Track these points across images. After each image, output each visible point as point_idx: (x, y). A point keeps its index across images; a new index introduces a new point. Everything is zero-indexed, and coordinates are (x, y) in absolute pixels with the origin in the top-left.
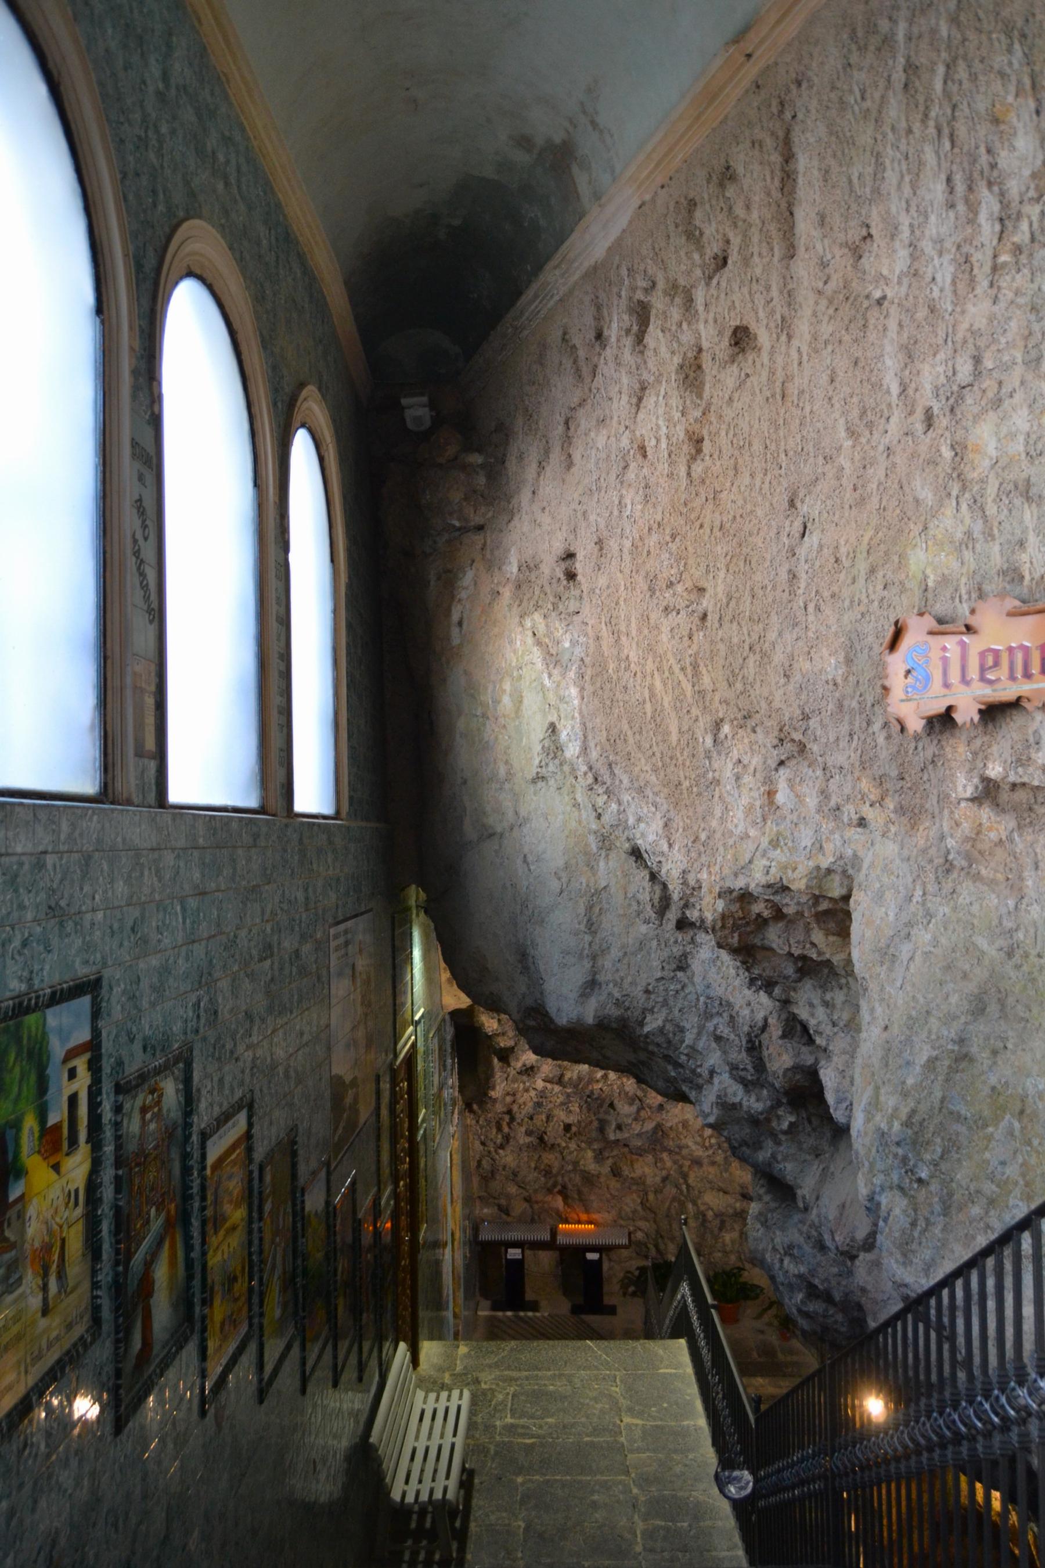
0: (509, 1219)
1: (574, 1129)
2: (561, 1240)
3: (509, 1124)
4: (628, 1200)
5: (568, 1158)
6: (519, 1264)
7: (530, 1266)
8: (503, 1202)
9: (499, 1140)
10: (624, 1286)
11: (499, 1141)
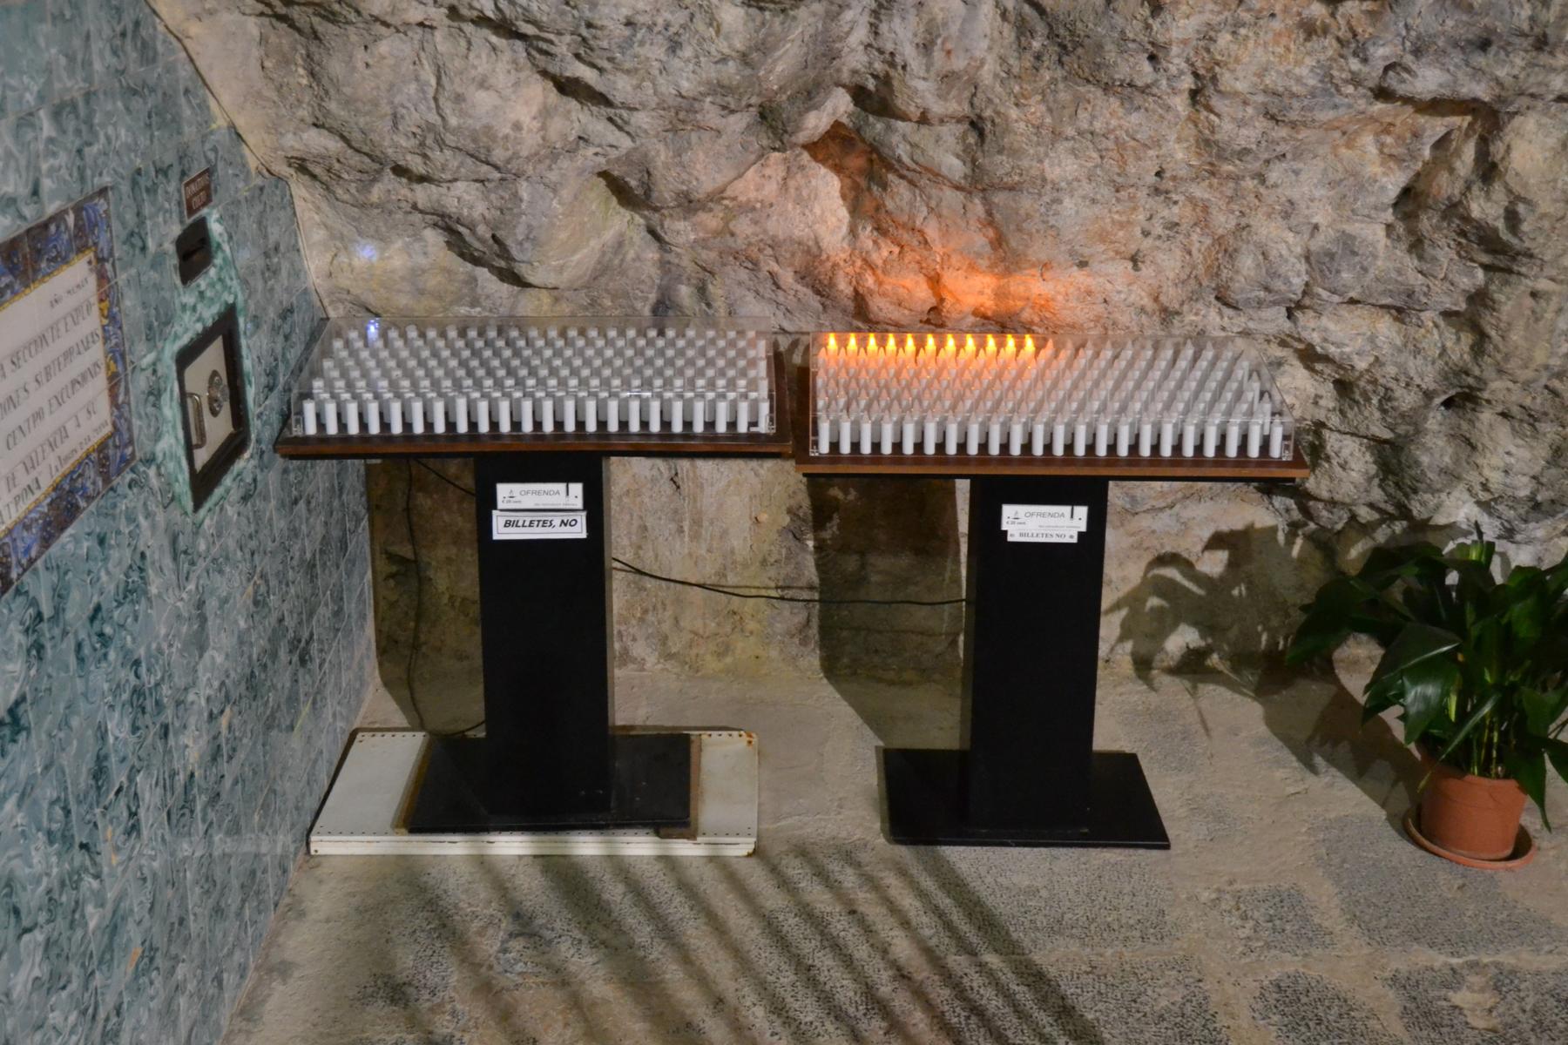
0: (528, 304)
2: (838, 428)
6: (576, 570)
10: (1146, 631)
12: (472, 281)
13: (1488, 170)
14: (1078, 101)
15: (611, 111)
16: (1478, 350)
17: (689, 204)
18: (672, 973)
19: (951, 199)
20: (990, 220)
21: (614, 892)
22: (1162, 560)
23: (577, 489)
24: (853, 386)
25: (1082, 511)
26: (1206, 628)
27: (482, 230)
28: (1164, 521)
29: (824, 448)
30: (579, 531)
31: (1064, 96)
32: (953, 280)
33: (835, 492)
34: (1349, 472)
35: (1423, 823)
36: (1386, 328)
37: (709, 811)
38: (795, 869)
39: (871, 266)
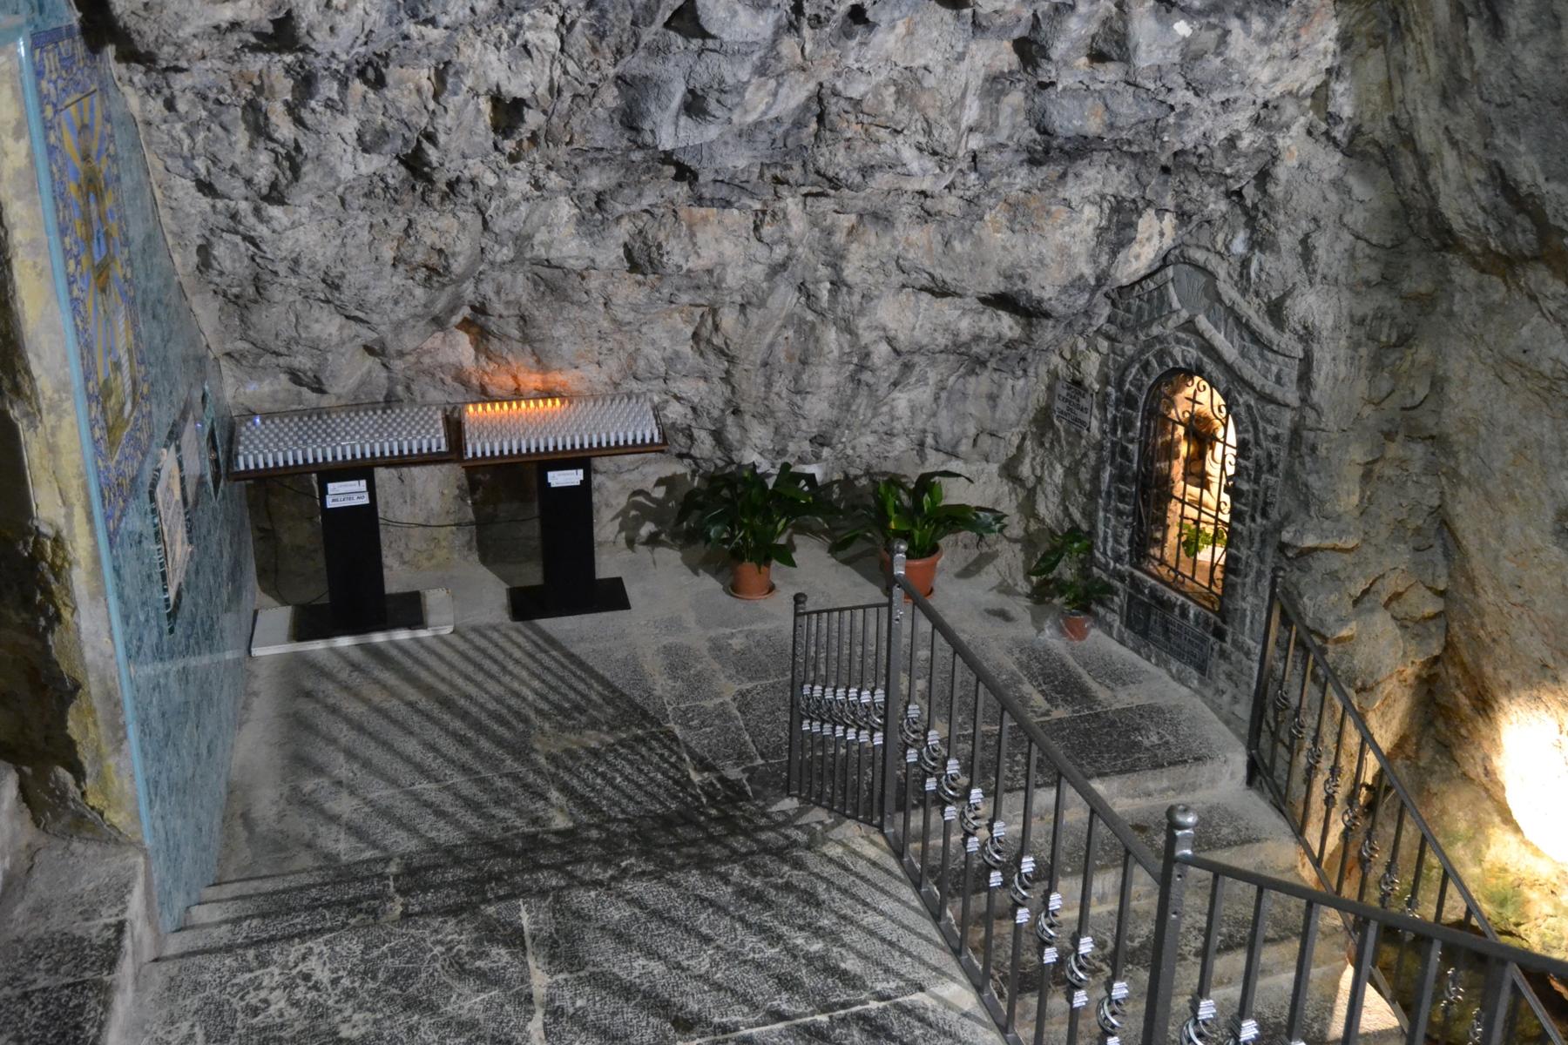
0: (325, 402)
1: (533, 119)
2: (475, 446)
3: (292, 110)
4: (658, 332)
5: (501, 224)
6: (364, 520)
7: (393, 508)
8: (303, 361)
9: (264, 170)
10: (629, 525)
11: (263, 177)
12: (299, 393)
13: (716, 327)
14: (562, 308)
15: (272, 145)
16: (733, 392)
17: (401, 354)
18: (424, 674)
19: (517, 346)
20: (534, 353)
21: (394, 652)
22: (635, 493)
23: (363, 482)
24: (481, 426)
25: (581, 472)
26: (657, 522)
27: (310, 374)
28: (635, 475)
29: (470, 455)
30: (366, 500)
31: (556, 306)
32: (523, 377)
33: (479, 476)
34: (705, 445)
35: (734, 589)
36: (702, 384)
37: (431, 619)
38: (472, 636)
39: (485, 372)
